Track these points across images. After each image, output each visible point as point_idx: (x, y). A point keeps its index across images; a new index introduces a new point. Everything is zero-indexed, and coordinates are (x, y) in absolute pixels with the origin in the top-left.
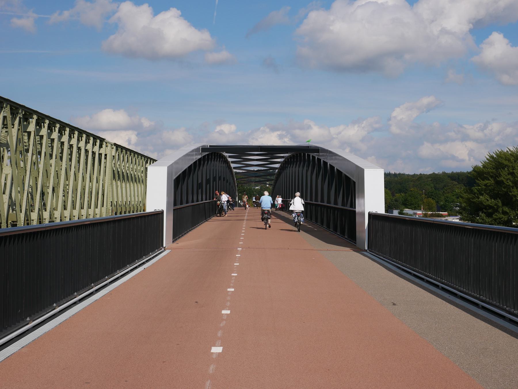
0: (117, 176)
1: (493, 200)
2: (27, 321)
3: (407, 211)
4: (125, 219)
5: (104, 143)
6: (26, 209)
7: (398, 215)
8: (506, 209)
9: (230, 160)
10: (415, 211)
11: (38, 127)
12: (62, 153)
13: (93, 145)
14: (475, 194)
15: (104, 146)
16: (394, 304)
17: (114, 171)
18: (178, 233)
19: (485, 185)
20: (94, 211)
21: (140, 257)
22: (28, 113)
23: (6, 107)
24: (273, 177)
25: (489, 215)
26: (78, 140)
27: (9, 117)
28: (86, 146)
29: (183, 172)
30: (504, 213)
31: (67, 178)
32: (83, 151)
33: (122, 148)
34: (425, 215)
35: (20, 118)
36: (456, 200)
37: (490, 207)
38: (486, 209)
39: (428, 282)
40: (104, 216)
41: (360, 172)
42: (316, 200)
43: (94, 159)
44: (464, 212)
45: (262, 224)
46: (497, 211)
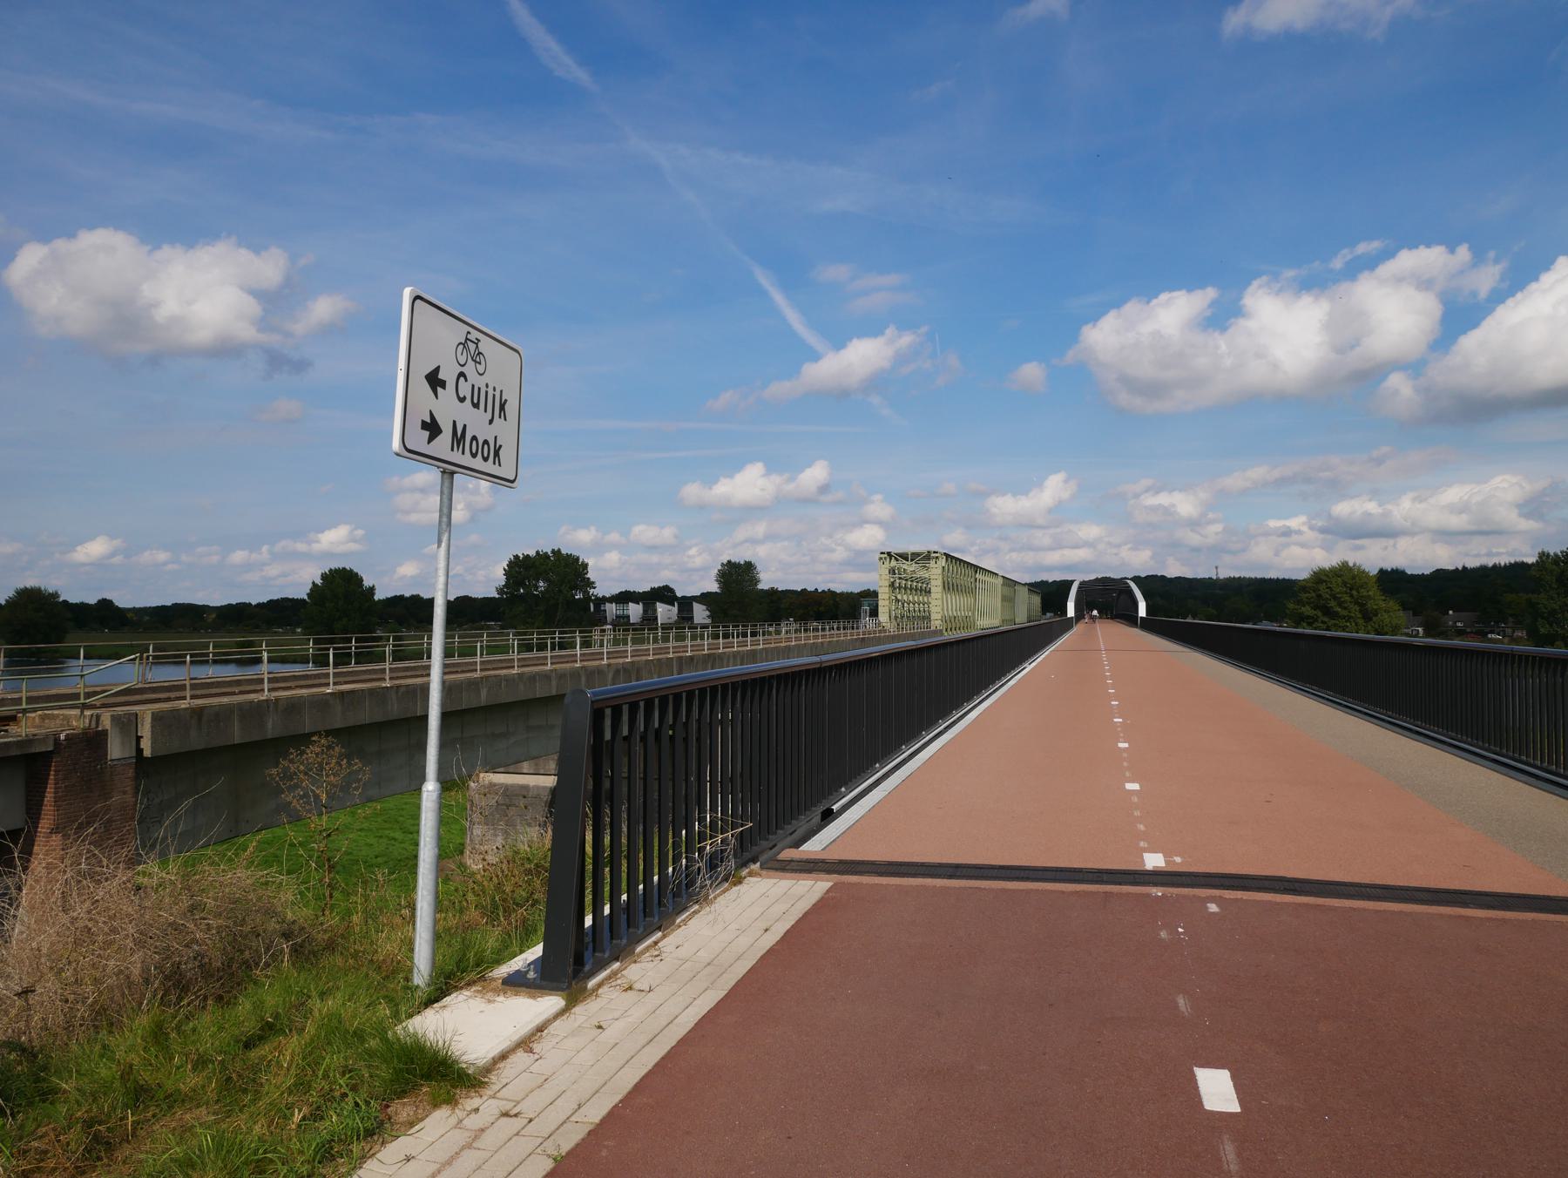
2: (876, 768)
8: (1326, 619)
46: (1316, 620)
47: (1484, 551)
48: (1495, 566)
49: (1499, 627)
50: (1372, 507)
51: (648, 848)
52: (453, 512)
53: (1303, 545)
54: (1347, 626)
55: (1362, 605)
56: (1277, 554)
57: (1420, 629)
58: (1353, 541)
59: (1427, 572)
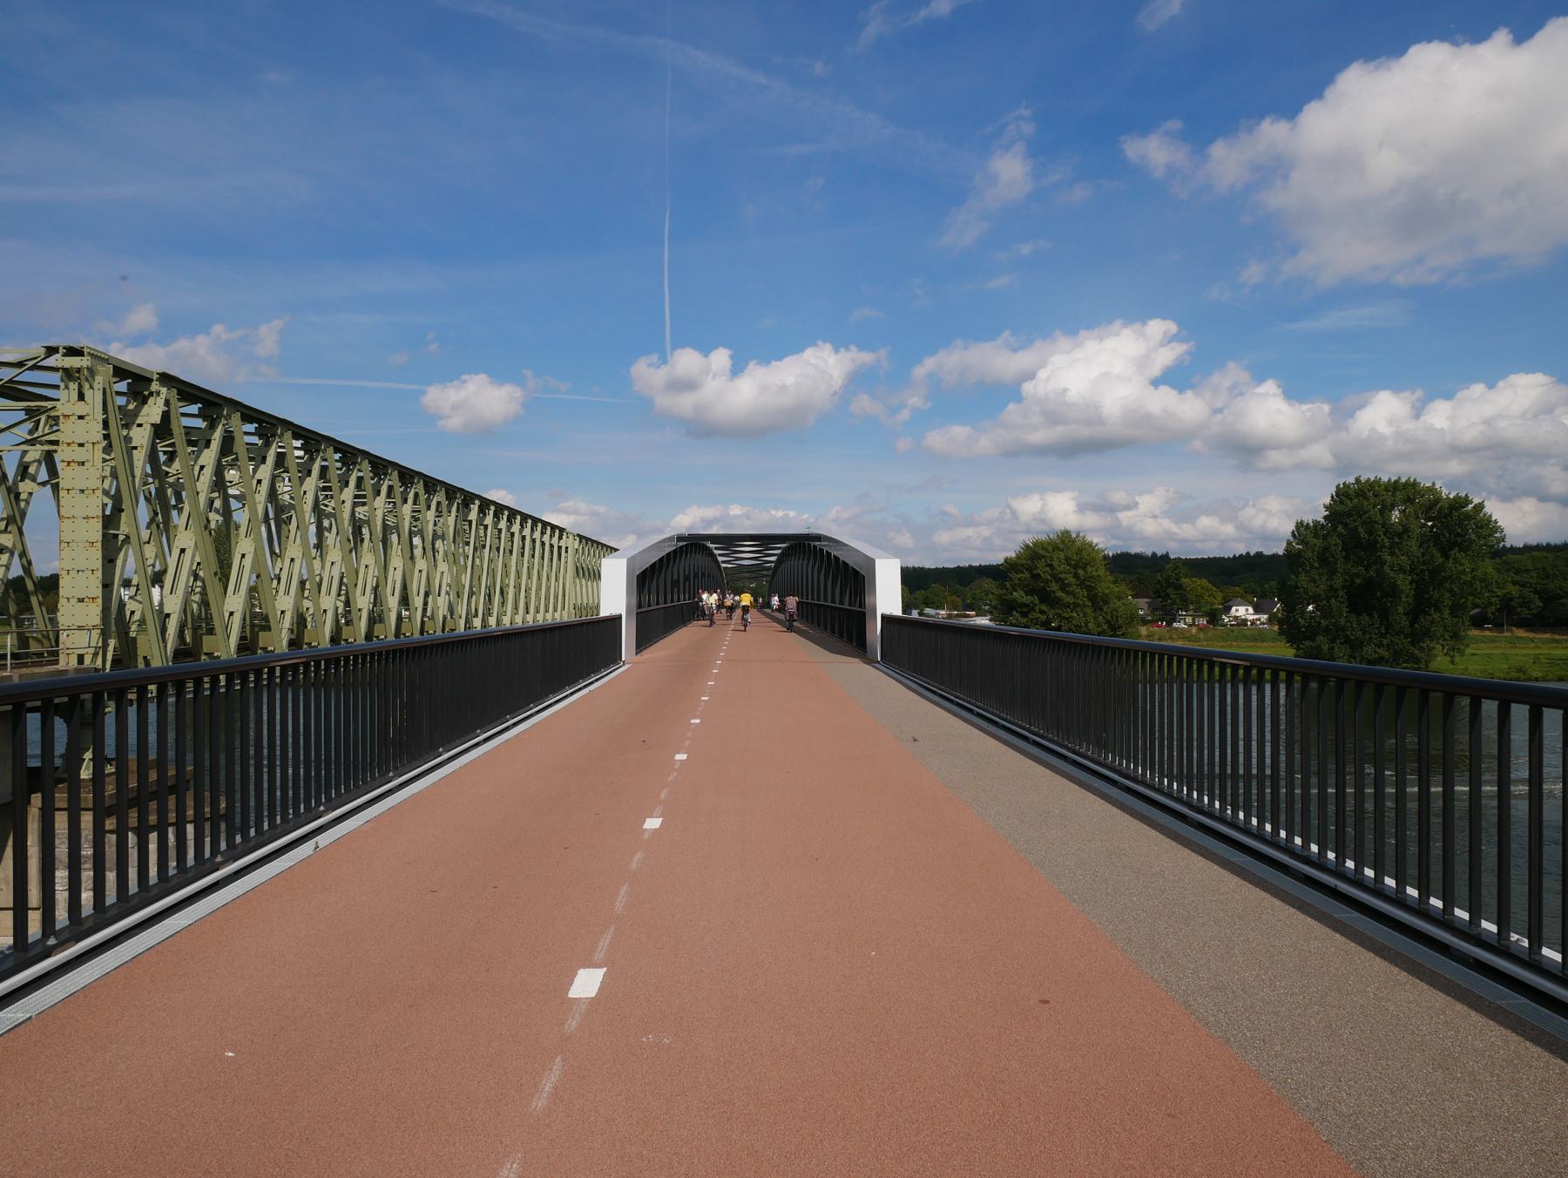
0: (587, 573)
1: (1029, 597)
3: (928, 610)
4: (594, 622)
5: (565, 534)
6: (483, 613)
7: (917, 616)
8: (1044, 607)
9: (716, 552)
10: (938, 611)
11: (481, 515)
12: (523, 548)
13: (551, 536)
14: (1006, 589)
15: (564, 537)
16: (915, 740)
17: (577, 567)
18: (642, 643)
19: (1019, 579)
20: (561, 614)
21: (588, 675)
22: (469, 498)
23: (419, 482)
24: (770, 573)
25: (1024, 615)
26: (532, 530)
27: (445, 503)
28: (551, 540)
29: (651, 566)
30: (1042, 612)
31: (529, 577)
32: (538, 544)
33: (588, 539)
34: (950, 616)
35: (458, 504)
36: (985, 598)
37: (1026, 605)
38: (1020, 608)
39: (958, 705)
40: (566, 619)
41: (871, 563)
42: (826, 600)
43: (552, 552)
44: (995, 611)
45: (743, 628)
51: (259, 864)
55: (1089, 588)
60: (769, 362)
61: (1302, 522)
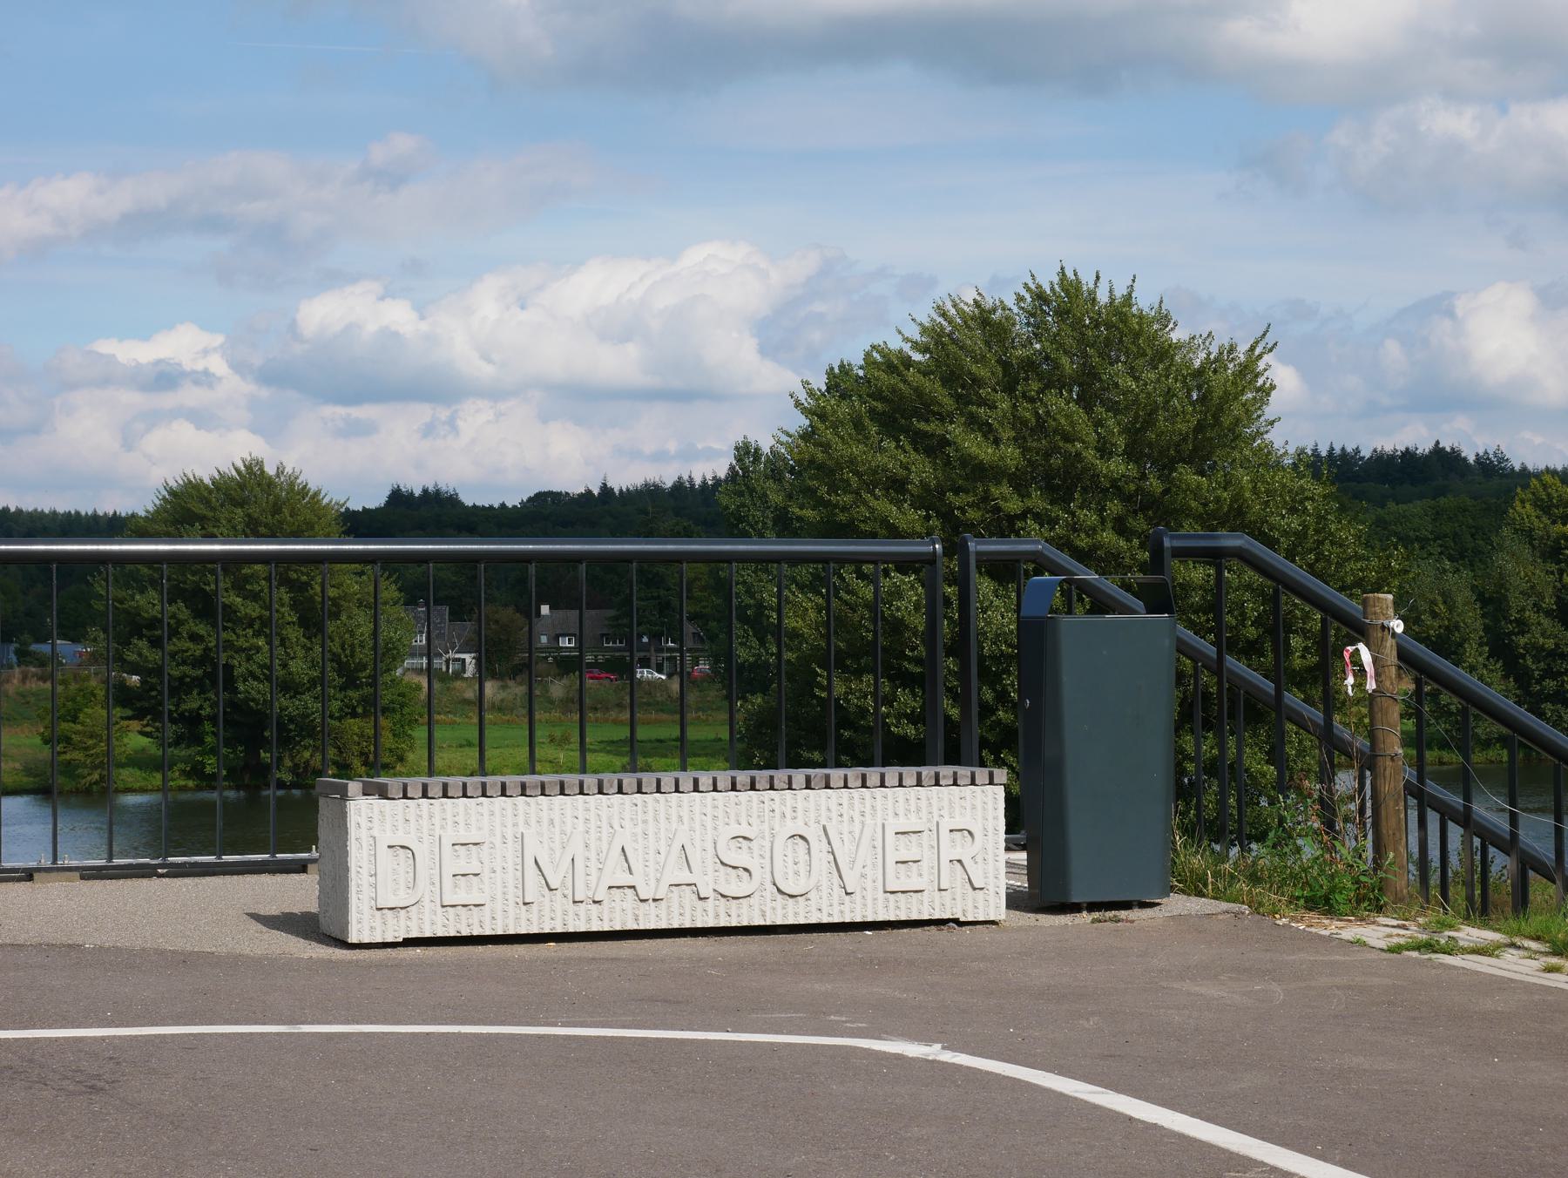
8: (201, 629)
30: (195, 638)
47: (672, 447)
48: (679, 486)
49: (661, 650)
50: (399, 316)
52: (980, 920)
53: (201, 419)
54: (258, 649)
56: (128, 443)
57: (468, 657)
58: (341, 411)
59: (513, 501)
60: (937, 340)
61: (746, 445)
